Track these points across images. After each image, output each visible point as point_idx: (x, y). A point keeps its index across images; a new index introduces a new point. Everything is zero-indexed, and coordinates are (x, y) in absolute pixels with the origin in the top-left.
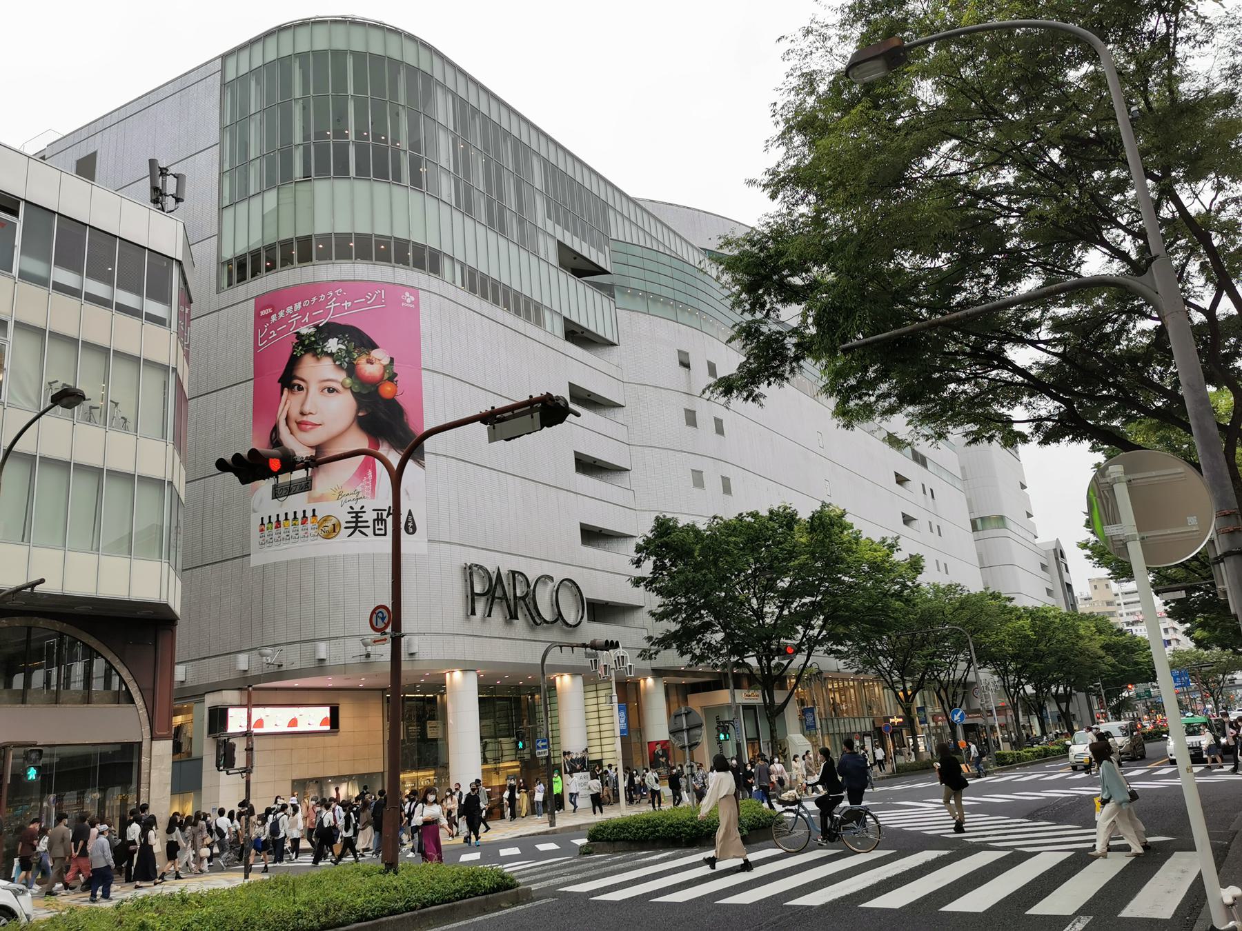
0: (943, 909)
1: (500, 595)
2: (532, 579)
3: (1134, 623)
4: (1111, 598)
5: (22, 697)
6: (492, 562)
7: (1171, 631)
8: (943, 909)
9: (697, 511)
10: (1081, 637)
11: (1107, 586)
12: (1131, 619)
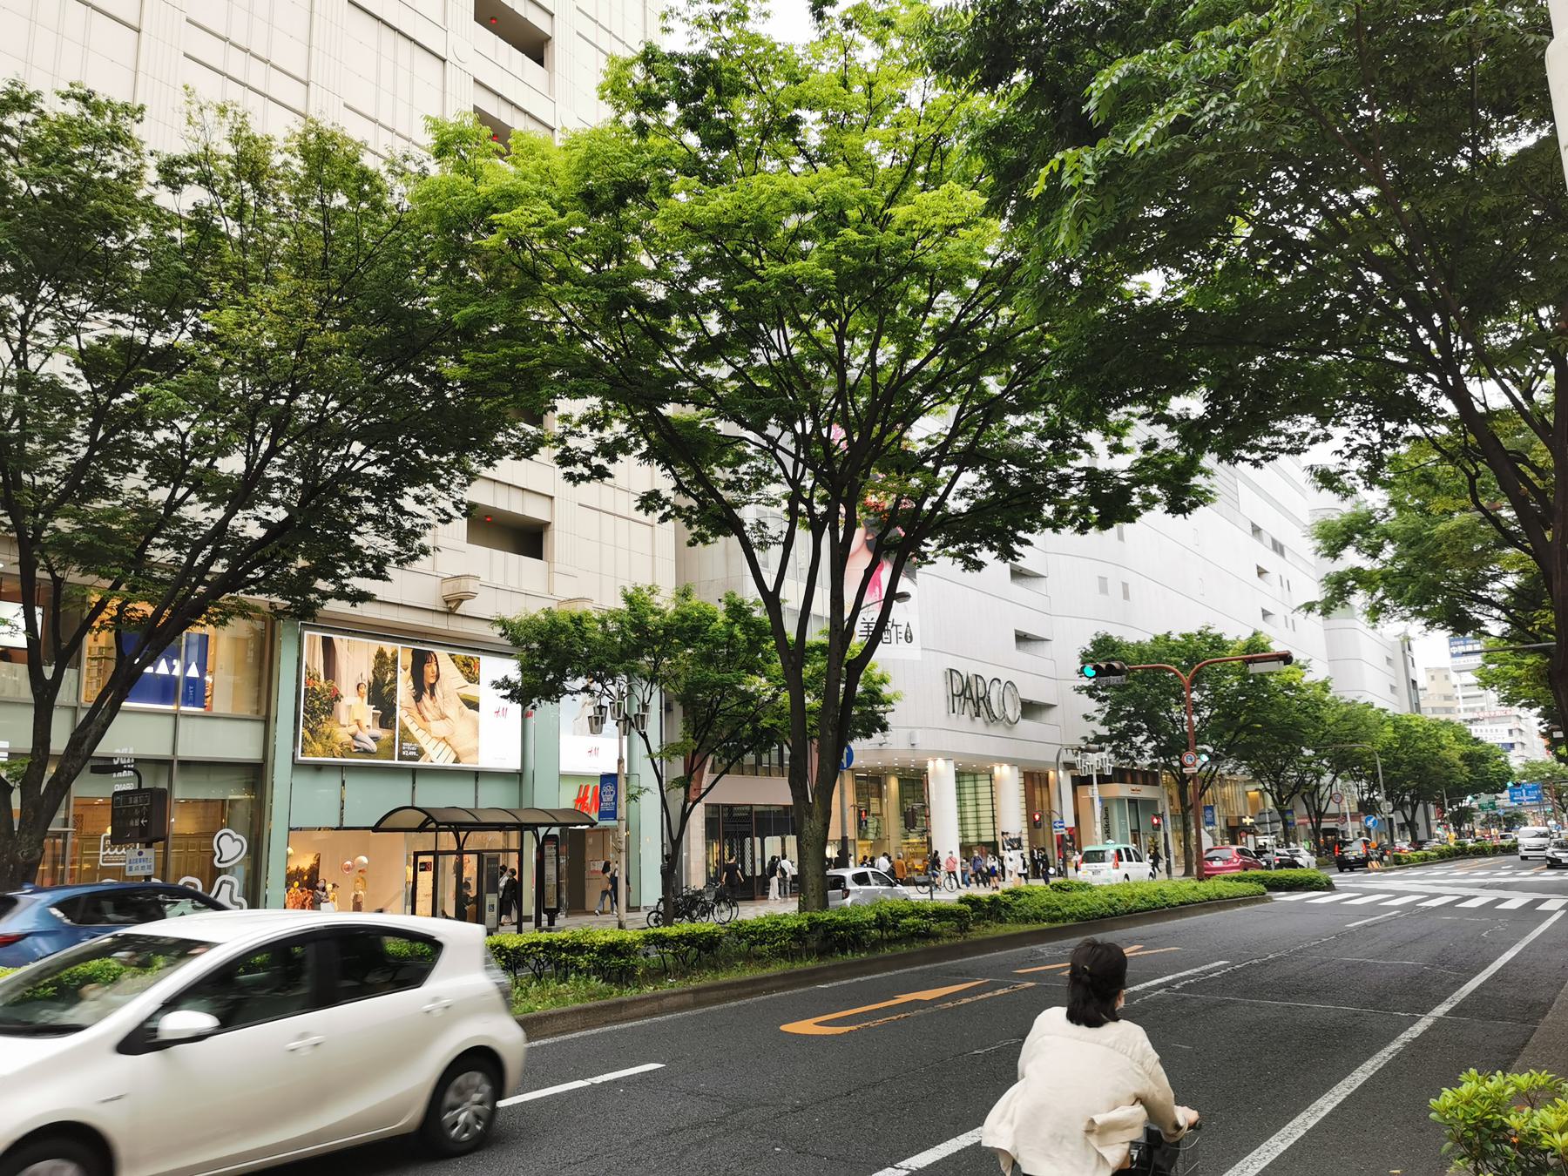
0: (783, 1028)
1: (970, 696)
2: (988, 679)
3: (1471, 722)
4: (1450, 692)
5: (755, 770)
6: (968, 669)
7: (1516, 733)
8: (783, 1028)
9: (1138, 628)
10: (1442, 747)
11: (1447, 677)
12: (1469, 716)
